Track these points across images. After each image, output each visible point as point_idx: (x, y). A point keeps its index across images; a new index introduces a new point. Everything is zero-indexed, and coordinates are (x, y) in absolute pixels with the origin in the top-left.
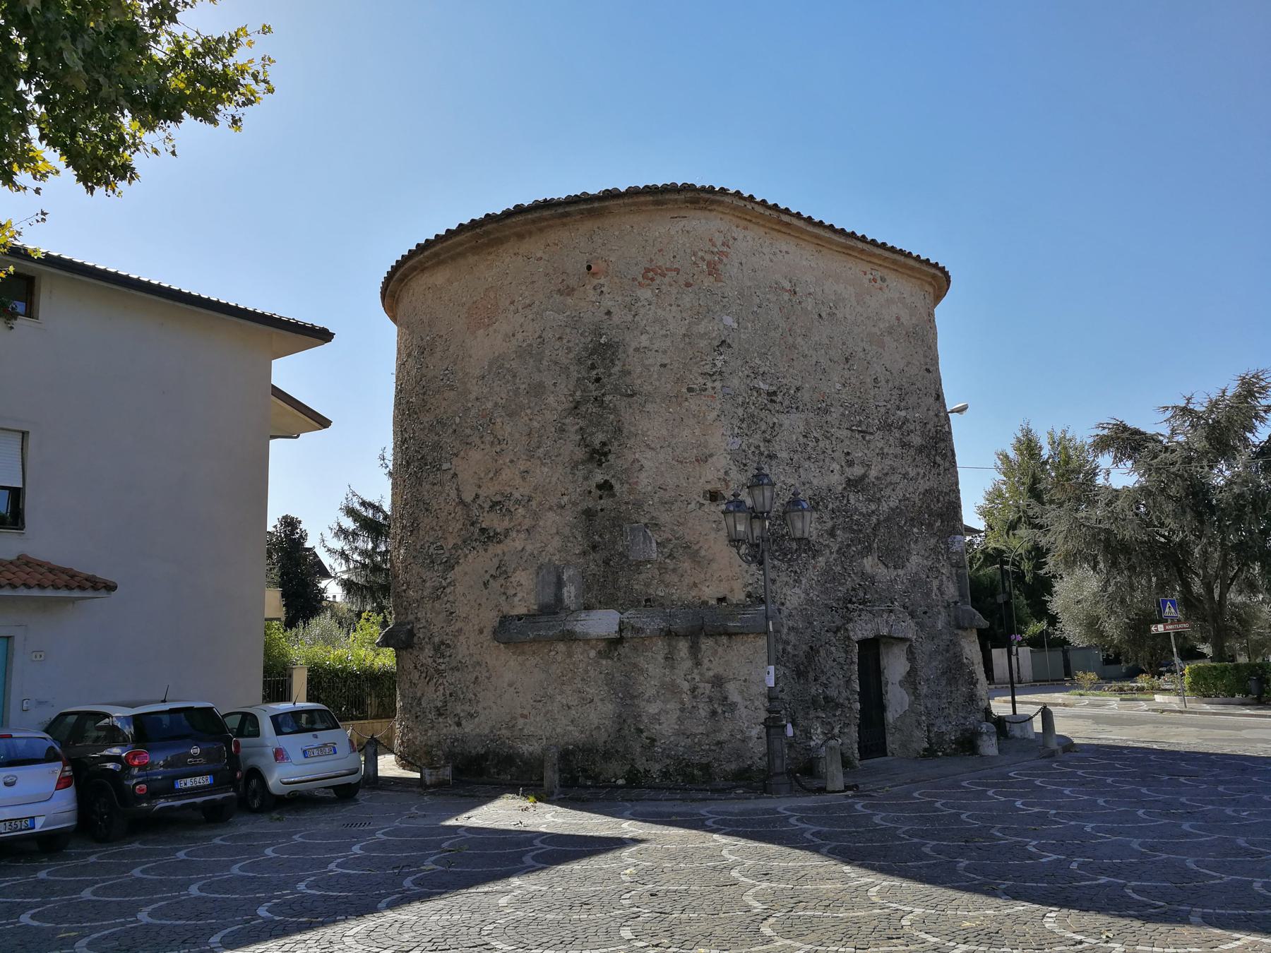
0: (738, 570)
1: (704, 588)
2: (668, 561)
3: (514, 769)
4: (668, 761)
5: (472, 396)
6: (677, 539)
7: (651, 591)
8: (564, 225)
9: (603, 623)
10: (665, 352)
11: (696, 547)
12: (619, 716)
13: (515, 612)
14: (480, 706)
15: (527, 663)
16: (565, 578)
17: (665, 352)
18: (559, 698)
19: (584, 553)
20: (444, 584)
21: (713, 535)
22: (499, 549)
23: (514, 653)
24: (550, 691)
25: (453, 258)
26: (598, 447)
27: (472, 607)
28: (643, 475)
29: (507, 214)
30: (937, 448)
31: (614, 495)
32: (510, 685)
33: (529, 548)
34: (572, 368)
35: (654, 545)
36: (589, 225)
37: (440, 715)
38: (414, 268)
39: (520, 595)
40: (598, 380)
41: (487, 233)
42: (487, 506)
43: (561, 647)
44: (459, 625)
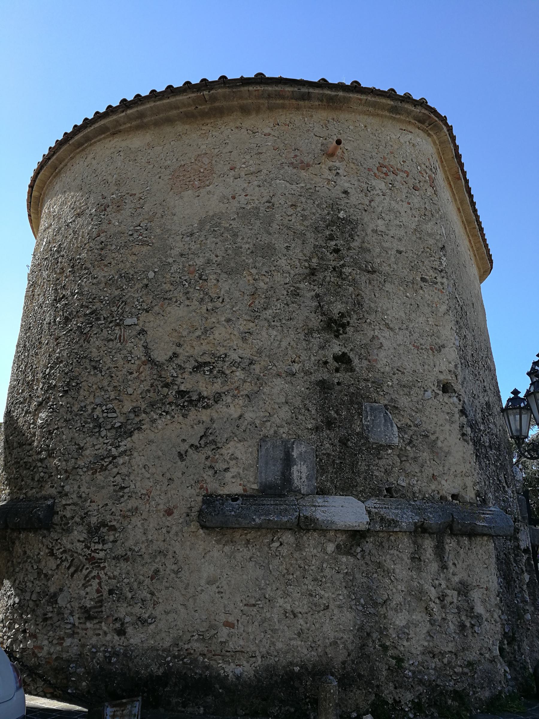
0: (468, 466)
1: (443, 482)
2: (408, 448)
3: (210, 699)
4: (421, 688)
5: (175, 252)
6: (416, 426)
7: (391, 480)
8: (298, 108)
9: (347, 511)
10: (400, 240)
11: (433, 437)
12: (361, 629)
13: (225, 491)
14: (160, 608)
15: (238, 556)
16: (295, 454)
17: (400, 240)
18: (281, 601)
19: (317, 429)
20: (114, 452)
21: (447, 427)
22: (204, 415)
23: (218, 542)
24: (269, 593)
25: (157, 124)
26: (336, 317)
27: (156, 482)
28: (382, 354)
29: (244, 81)
30: (500, 400)
31: (352, 370)
32: (210, 582)
33: (249, 416)
34: (308, 235)
35: (395, 429)
36: (322, 115)
37: (89, 618)
38: (103, 130)
39: (234, 471)
40: (337, 251)
41: (214, 99)
42: (189, 367)
43: (288, 537)
44: (133, 503)
